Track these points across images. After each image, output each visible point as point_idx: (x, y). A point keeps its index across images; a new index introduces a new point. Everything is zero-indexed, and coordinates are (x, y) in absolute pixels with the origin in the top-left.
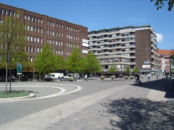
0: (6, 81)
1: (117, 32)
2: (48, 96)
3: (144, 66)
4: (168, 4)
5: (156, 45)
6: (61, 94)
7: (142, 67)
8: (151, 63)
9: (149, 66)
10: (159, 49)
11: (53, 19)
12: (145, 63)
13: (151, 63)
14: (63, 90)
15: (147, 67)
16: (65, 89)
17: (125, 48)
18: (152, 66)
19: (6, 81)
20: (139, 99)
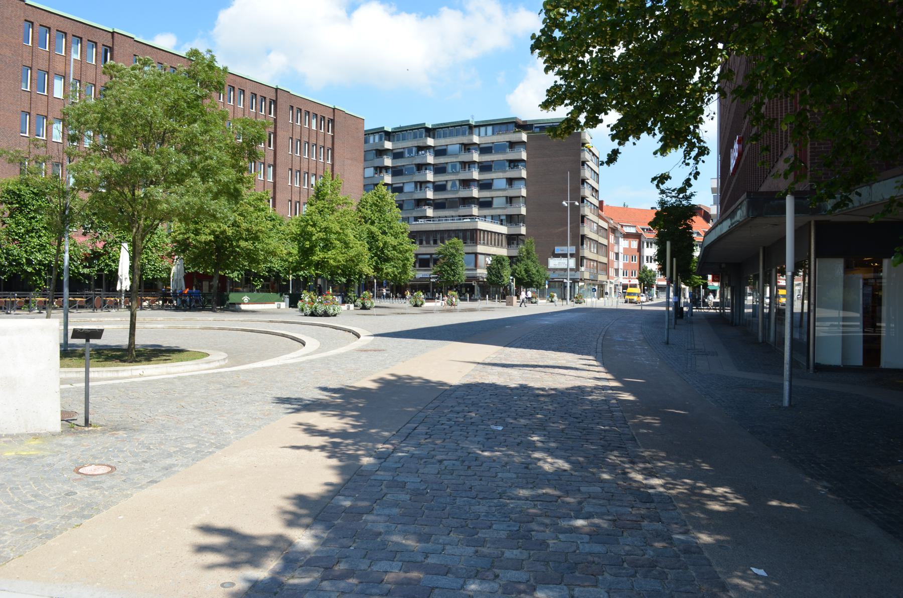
0: (63, 387)
1: (465, 140)
2: (512, 379)
3: (553, 263)
4: (548, 91)
5: (597, 191)
6: (307, 355)
7: (547, 264)
8: (578, 250)
9: (572, 263)
10: (605, 204)
11: (238, 79)
12: (558, 250)
13: (578, 250)
14: (312, 344)
15: (565, 267)
16: (318, 339)
17: (492, 198)
18: (580, 260)
19: (63, 387)
20: (61, 346)
